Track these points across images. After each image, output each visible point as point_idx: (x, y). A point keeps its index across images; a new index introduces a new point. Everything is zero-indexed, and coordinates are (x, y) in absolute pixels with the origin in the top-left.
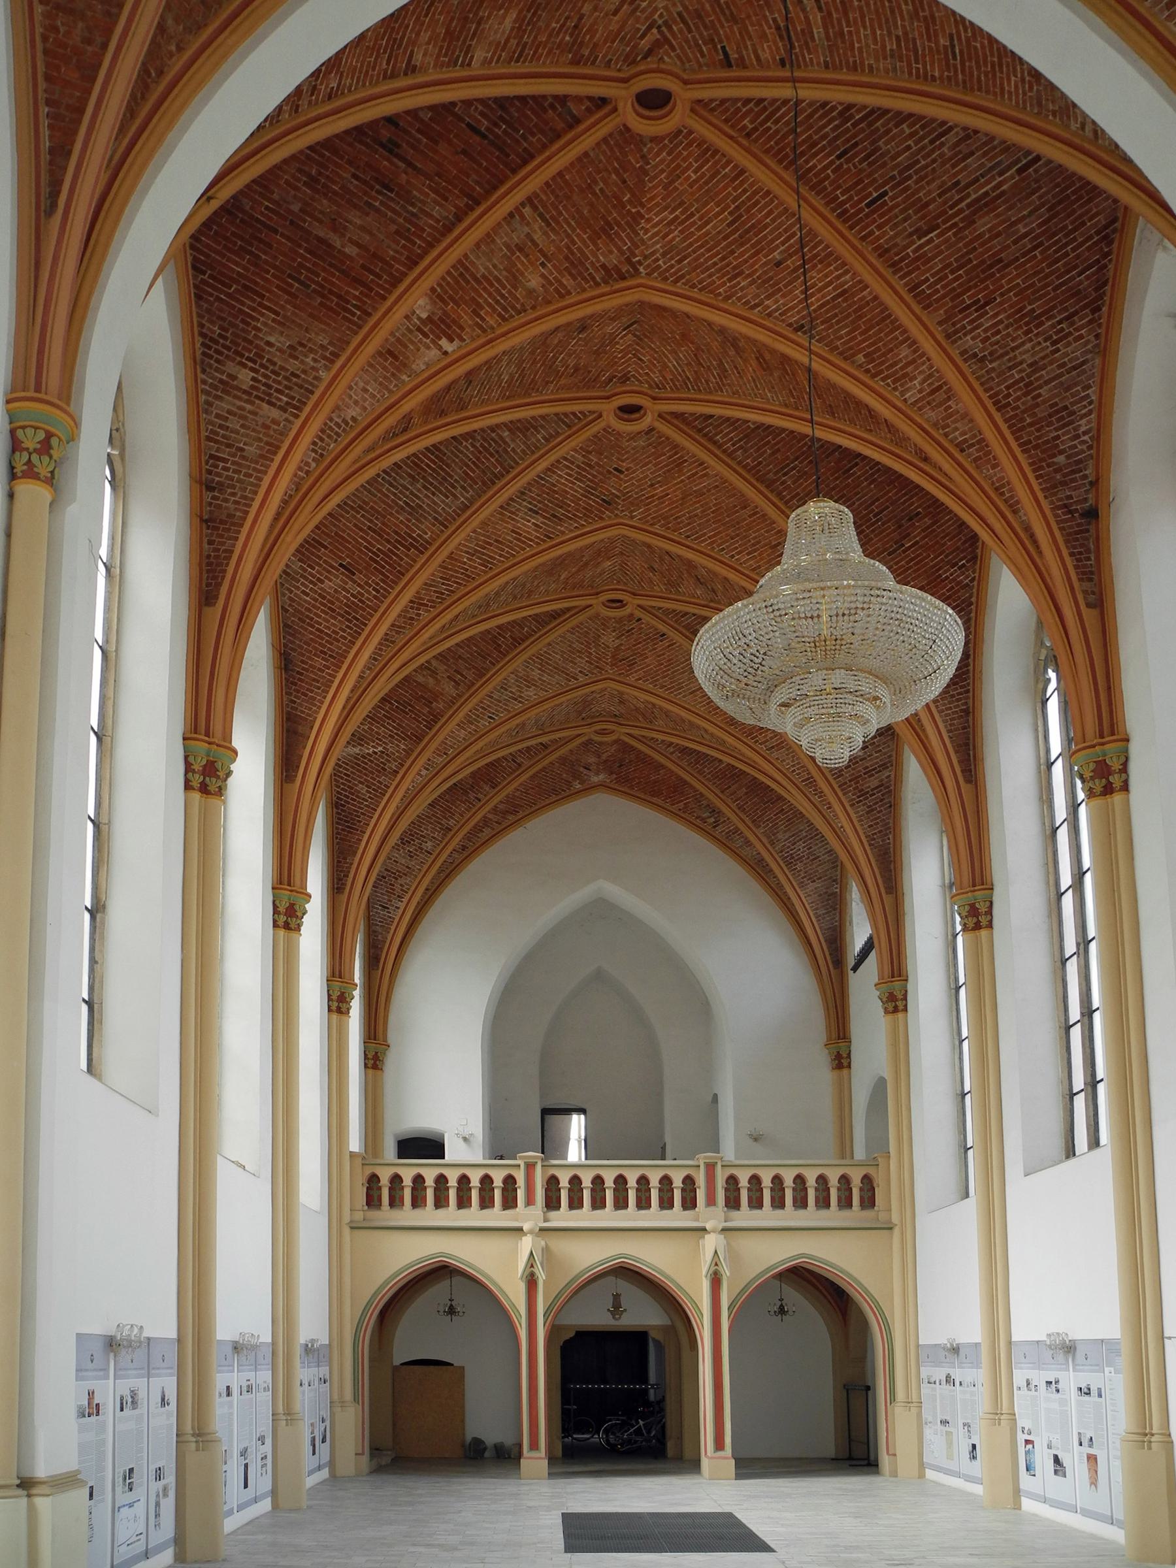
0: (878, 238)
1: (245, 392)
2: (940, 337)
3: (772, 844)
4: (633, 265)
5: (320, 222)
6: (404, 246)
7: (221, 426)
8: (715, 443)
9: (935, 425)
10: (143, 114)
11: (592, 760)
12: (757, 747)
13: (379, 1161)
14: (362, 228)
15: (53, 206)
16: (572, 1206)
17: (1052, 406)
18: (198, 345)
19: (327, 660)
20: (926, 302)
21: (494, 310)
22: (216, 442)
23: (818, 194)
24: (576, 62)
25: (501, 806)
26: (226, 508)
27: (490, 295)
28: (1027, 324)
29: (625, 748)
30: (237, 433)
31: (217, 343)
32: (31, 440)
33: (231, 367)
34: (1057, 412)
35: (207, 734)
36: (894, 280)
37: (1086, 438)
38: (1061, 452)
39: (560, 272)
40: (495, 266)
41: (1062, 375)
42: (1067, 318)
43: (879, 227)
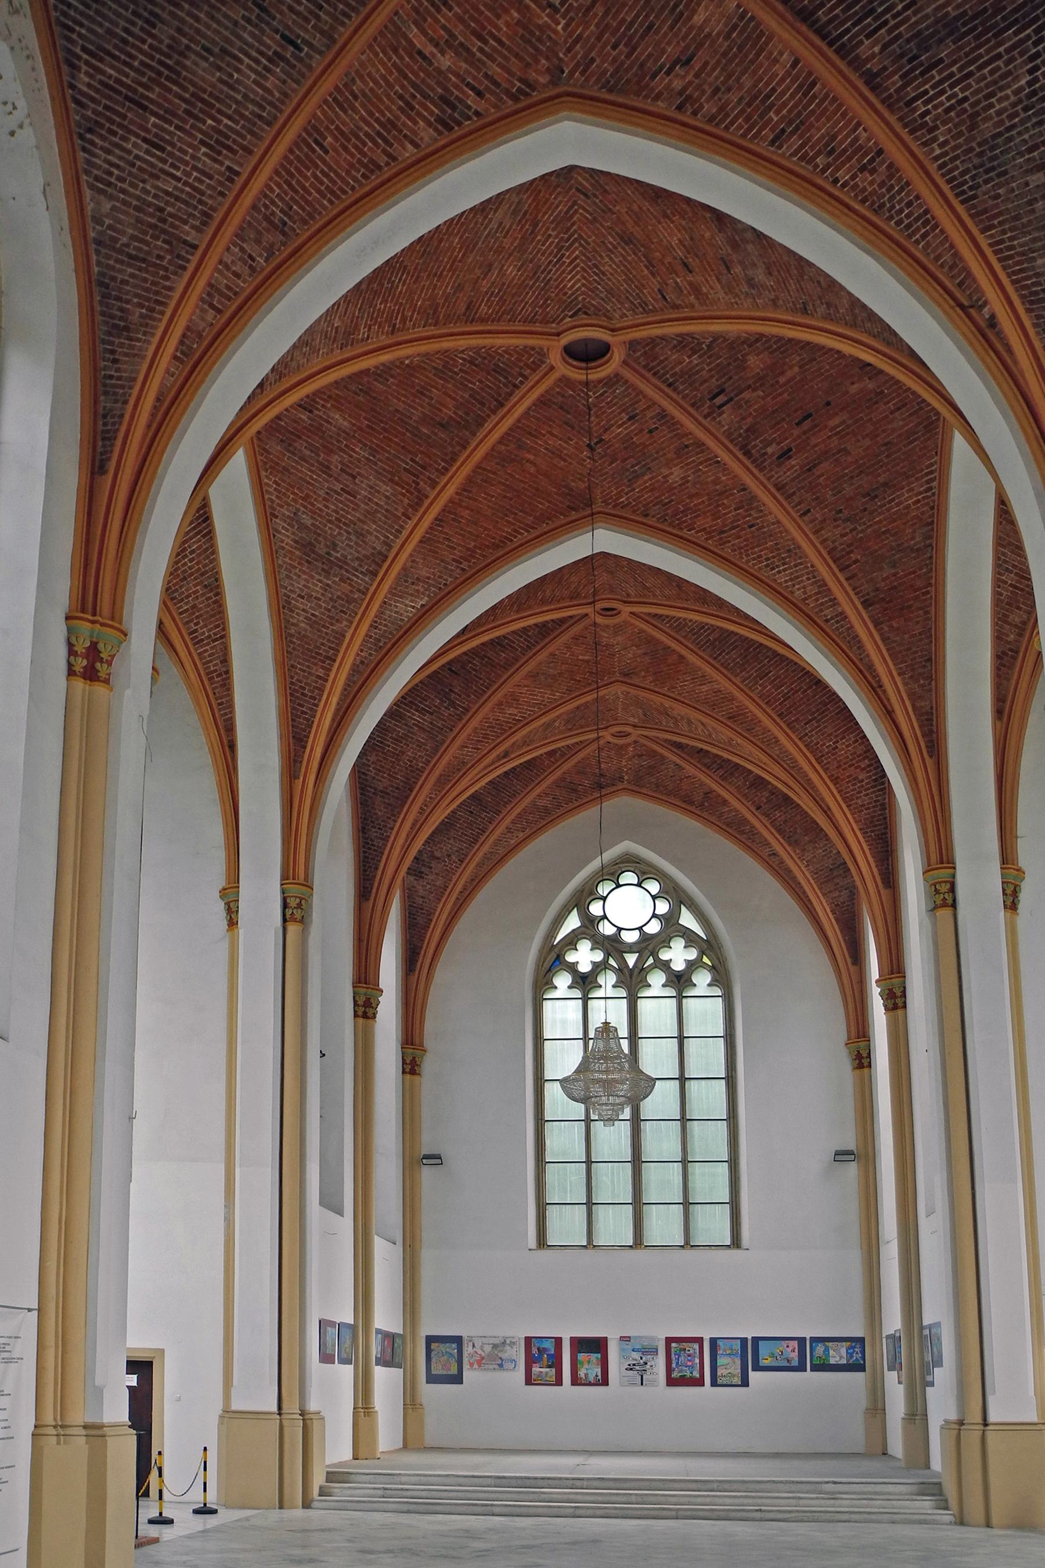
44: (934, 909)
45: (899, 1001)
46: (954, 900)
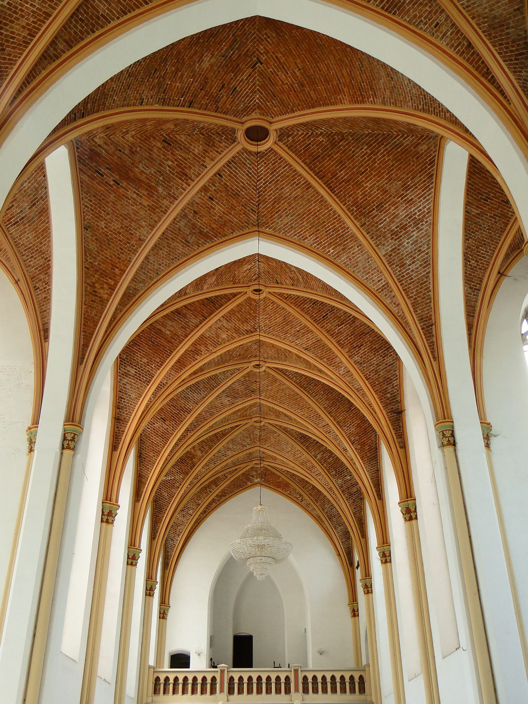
0: (326, 327)
1: (132, 376)
2: (347, 357)
3: (323, 509)
4: (255, 329)
5: (159, 324)
6: (184, 331)
7: (124, 387)
8: (286, 375)
9: (349, 382)
10: (108, 332)
11: (254, 473)
12: (312, 474)
13: (160, 670)
14: (171, 326)
15: (82, 361)
16: (239, 693)
17: (384, 378)
18: (119, 361)
19: (154, 453)
20: (342, 347)
21: (212, 345)
22: (122, 392)
23: (307, 314)
24: (234, 283)
25: (220, 494)
26: (124, 416)
27: (210, 341)
28: (374, 352)
29: (267, 469)
30: (129, 390)
31: (125, 360)
32: (69, 437)
33: (129, 368)
34: (386, 380)
35: (110, 501)
36: (332, 339)
37: (396, 387)
38: (389, 393)
39: (232, 333)
40: (212, 334)
41: (387, 367)
42: (386, 350)
43: (326, 324)
44: (443, 446)
45: (413, 515)
46: (454, 441)
